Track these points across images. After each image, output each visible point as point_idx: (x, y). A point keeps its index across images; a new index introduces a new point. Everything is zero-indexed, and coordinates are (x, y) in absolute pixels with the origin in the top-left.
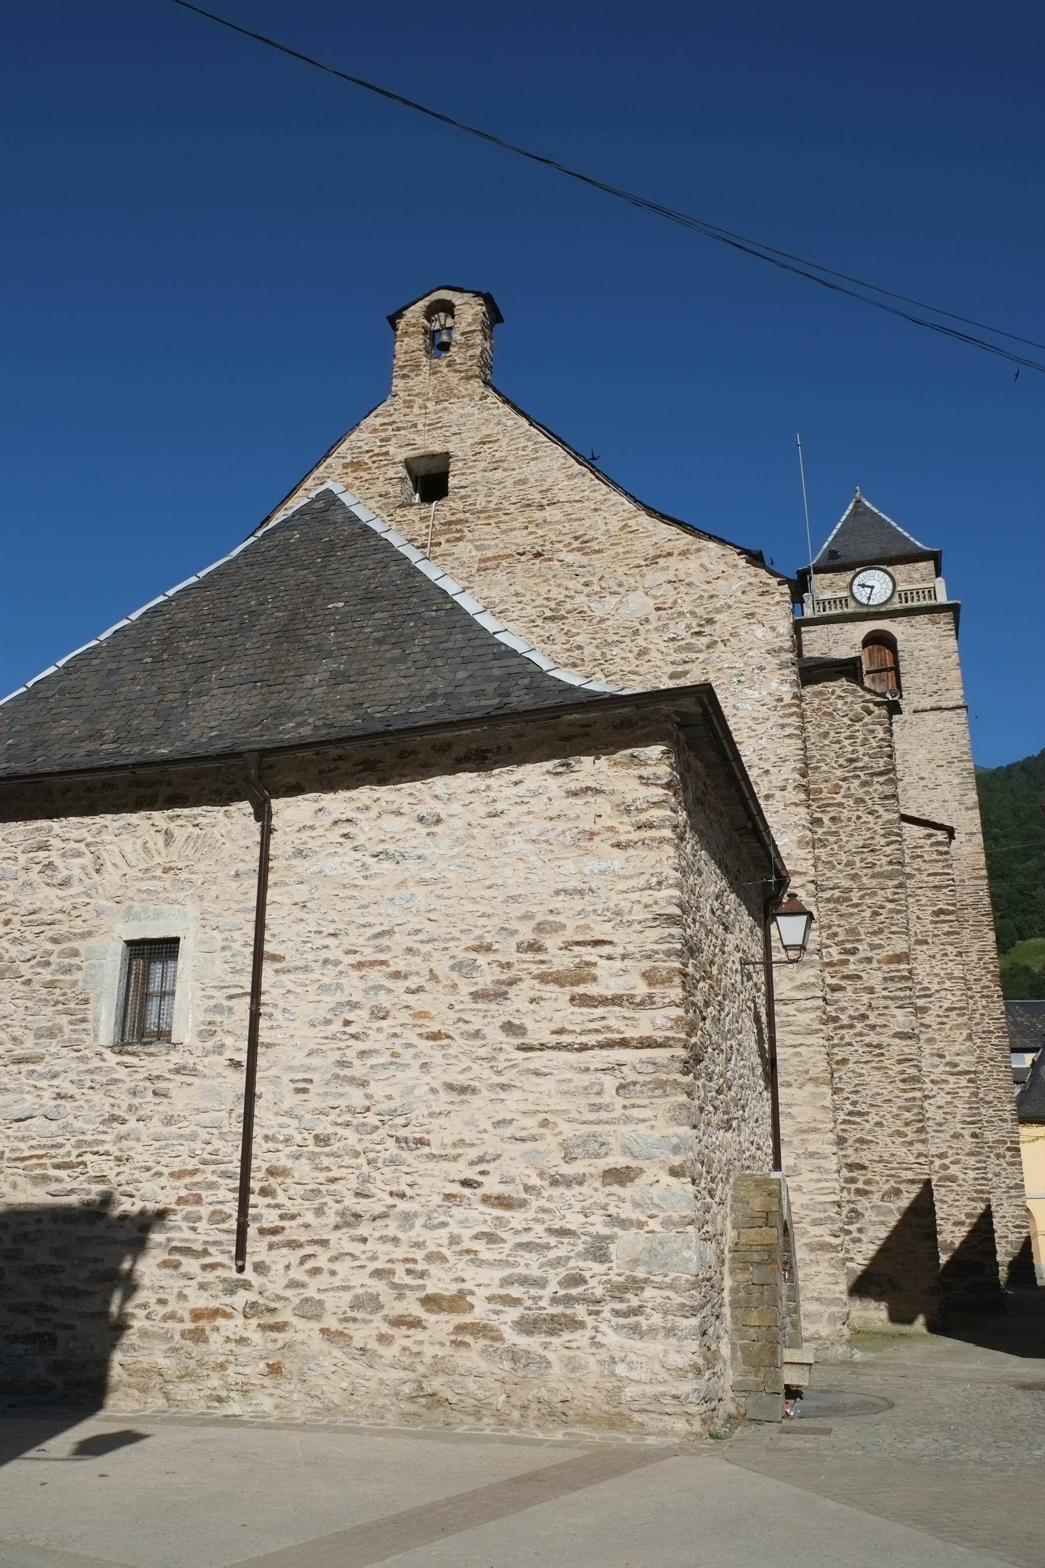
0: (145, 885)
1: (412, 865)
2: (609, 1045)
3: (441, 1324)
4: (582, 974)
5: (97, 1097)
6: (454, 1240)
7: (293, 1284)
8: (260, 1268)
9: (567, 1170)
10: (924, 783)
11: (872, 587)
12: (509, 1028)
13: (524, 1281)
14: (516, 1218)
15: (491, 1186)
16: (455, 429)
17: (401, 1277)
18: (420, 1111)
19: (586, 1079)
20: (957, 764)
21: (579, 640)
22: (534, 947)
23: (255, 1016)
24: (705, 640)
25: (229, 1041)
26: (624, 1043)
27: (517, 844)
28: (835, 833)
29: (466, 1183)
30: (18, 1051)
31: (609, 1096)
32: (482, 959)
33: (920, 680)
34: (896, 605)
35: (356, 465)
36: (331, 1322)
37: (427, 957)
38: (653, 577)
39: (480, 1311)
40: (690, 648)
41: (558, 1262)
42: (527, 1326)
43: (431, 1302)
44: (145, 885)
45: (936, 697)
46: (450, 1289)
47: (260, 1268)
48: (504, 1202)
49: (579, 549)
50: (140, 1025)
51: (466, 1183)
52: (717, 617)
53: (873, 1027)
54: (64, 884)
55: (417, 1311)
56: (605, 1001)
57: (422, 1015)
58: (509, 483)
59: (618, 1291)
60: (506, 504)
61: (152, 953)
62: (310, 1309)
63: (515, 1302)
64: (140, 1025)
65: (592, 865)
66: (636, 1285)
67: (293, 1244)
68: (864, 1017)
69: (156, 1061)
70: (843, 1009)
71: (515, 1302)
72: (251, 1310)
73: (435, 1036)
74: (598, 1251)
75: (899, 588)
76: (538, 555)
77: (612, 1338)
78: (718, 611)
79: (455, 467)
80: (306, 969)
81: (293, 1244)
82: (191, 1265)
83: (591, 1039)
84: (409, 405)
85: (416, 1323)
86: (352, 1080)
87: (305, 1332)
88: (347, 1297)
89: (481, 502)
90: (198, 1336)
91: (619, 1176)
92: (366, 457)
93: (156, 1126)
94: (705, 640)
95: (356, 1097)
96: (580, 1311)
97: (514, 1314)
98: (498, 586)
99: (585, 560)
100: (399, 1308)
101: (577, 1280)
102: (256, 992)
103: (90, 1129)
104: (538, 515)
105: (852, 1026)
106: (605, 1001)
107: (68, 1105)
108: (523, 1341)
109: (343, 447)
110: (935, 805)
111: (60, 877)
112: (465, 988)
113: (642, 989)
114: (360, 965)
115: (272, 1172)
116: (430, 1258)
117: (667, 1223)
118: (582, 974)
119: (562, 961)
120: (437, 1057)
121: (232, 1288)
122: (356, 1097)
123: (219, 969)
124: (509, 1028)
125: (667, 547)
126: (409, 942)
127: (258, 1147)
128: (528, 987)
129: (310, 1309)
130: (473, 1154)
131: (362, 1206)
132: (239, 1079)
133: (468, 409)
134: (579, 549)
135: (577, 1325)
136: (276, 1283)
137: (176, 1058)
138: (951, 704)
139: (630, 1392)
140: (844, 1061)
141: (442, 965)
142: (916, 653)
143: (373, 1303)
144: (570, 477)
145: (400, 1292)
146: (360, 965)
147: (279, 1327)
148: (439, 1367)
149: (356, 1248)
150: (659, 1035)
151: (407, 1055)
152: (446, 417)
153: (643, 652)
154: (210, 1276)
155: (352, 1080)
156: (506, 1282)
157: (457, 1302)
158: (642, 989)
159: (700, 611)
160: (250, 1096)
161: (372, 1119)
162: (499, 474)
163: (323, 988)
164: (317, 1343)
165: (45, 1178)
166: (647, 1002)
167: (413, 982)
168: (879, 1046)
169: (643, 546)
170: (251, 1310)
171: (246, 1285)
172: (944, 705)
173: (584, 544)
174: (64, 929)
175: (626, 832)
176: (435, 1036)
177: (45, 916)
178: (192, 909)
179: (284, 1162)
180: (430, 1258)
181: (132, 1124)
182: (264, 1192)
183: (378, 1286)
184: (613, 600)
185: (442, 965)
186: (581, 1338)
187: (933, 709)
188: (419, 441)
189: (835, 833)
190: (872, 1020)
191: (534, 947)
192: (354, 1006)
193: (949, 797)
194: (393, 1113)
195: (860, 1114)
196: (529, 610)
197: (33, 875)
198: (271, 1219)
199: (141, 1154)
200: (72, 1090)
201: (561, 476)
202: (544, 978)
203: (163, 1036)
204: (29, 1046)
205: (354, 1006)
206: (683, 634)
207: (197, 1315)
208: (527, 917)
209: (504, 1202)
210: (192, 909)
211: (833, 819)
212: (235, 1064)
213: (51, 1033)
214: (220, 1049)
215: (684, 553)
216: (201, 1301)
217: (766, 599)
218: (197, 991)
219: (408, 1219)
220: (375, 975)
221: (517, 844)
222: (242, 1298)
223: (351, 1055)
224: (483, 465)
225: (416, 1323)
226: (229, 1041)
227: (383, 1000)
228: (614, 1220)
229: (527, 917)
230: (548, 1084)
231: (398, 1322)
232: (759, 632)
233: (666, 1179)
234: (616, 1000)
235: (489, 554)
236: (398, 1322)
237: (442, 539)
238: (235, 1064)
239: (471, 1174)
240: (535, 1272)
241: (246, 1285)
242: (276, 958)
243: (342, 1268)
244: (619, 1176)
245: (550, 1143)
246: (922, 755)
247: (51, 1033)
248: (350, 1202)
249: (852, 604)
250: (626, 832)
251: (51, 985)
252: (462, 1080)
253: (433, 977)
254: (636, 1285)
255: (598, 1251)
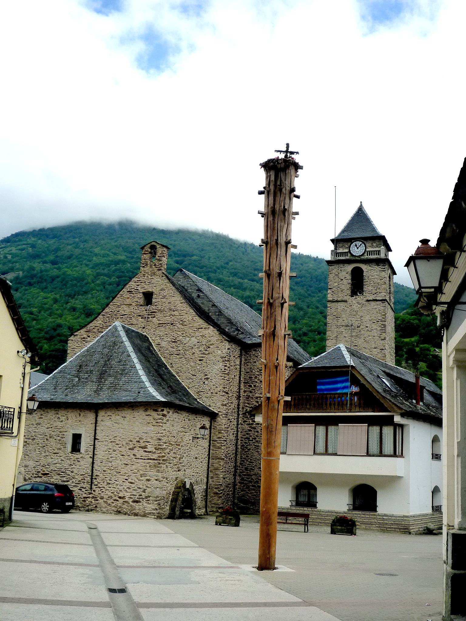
0: (76, 423)
1: (121, 425)
2: (148, 459)
3: (121, 501)
4: (145, 447)
5: (68, 461)
6: (124, 488)
7: (99, 494)
8: (94, 491)
9: (141, 478)
10: (367, 329)
11: (358, 248)
12: (134, 455)
13: (133, 495)
14: (133, 485)
15: (130, 480)
16: (155, 285)
17: (115, 493)
18: (119, 468)
19: (145, 464)
20: (380, 322)
21: (180, 348)
22: (138, 442)
23: (94, 449)
24: (207, 352)
25: (90, 453)
26: (151, 459)
27: (137, 423)
28: (254, 390)
29: (126, 479)
30: (54, 452)
31: (148, 468)
32: (131, 443)
33: (370, 288)
34: (366, 257)
35: (130, 292)
36: (105, 500)
37: (122, 442)
38: (197, 334)
39: (127, 499)
40: (204, 354)
41: (138, 493)
42: (134, 501)
43: (120, 497)
44: (76, 423)
45: (375, 295)
46: (122, 496)
47: (94, 491)
48: (131, 483)
49: (182, 324)
50: (76, 448)
51: (126, 479)
52: (211, 346)
53: (257, 441)
54: (62, 421)
55: (118, 499)
56: (149, 452)
57: (121, 451)
58: (167, 303)
59: (146, 497)
60: (165, 309)
61: (77, 438)
62: (102, 498)
63: (132, 498)
64: (76, 448)
65: (149, 428)
66: (149, 497)
67: (99, 487)
68: (255, 439)
69: (77, 455)
70: (251, 436)
71: (132, 498)
72: (93, 498)
73: (123, 455)
74: (144, 491)
75: (367, 250)
76: (172, 324)
77: (145, 504)
78: (211, 345)
79: (154, 296)
80: (102, 442)
81: (99, 487)
82: (83, 490)
83: (146, 458)
84: (144, 275)
85: (117, 500)
86: (109, 461)
87: (101, 501)
88: (107, 496)
89: (160, 307)
90: (84, 501)
91: (148, 480)
92: (133, 290)
93: (78, 467)
94: (207, 352)
95: (110, 464)
96: (141, 500)
97: (132, 500)
98: (161, 331)
99: (183, 327)
100: (115, 498)
101: (141, 495)
102: (94, 445)
103: (67, 466)
104: (173, 313)
105: (252, 441)
106: (149, 452)
107: (63, 462)
108: (132, 504)
109: (127, 286)
110: (370, 337)
111: (61, 420)
112: (128, 448)
113: (154, 450)
114: (111, 442)
115: (96, 476)
116: (120, 491)
117: (154, 488)
118: (145, 447)
119: (143, 445)
120: (123, 459)
121: (90, 493)
122: (110, 464)
123: (88, 440)
124: (134, 455)
125: (202, 326)
126: (119, 439)
127: (94, 471)
128: (137, 448)
129: (102, 498)
130: (127, 475)
131: (110, 482)
132: (91, 460)
133: (159, 280)
134: (182, 324)
135: (140, 502)
136: (96, 493)
137: (81, 455)
138: (380, 298)
139: (147, 512)
140: (250, 449)
141: (124, 443)
142: (370, 277)
143: (111, 497)
144: (181, 303)
145: (115, 496)
146: (111, 442)
147: (97, 500)
148: (120, 507)
149: (109, 489)
150: (156, 458)
151: (118, 458)
152: (153, 281)
153: (194, 353)
154: (86, 492)
155: (109, 461)
156: (131, 495)
157: (123, 498)
158: (154, 450)
159: (207, 344)
160: (93, 463)
161: (112, 468)
162: (164, 300)
163: (106, 446)
164: (103, 503)
165: (59, 474)
166: (155, 453)
167: (120, 446)
168: (258, 446)
169: (196, 325)
170: (93, 498)
171: (92, 493)
172: (378, 298)
173: (183, 323)
174: (62, 430)
175: (154, 424)
176: (123, 455)
177: (58, 427)
178: (84, 429)
179: (98, 474)
180: (120, 491)
181: (74, 466)
182: (95, 479)
183: (112, 495)
184: (188, 339)
185: (124, 443)
186: (141, 504)
187: (374, 300)
188: (146, 287)
189: (254, 390)
190: (257, 439)
191: (138, 442)
192: (110, 449)
193: (376, 334)
194: (116, 467)
195: (252, 462)
196: (169, 339)
197: (56, 419)
198: (96, 483)
199: (75, 471)
200: (64, 459)
201: (179, 302)
202: (140, 447)
203: (79, 451)
204: (56, 451)
205: (110, 449)
206: (203, 350)
207: (84, 498)
208: (138, 436)
209: (131, 483)
210: (84, 429)
211: (255, 386)
212: (91, 457)
213: (60, 449)
214: (88, 454)
215: (205, 328)
216: (85, 496)
217: (221, 344)
218: (85, 444)
219: (117, 485)
220: (113, 444)
221: (137, 423)
222: (91, 496)
223: (109, 457)
224: (161, 296)
225: (117, 500)
226: (90, 453)
227: (115, 448)
228: (147, 487)
229: (138, 436)
230: (139, 465)
231: (115, 500)
232: (219, 352)
233: (155, 481)
234: (150, 452)
235: (161, 322)
236: (115, 500)
237: (150, 316)
238: (91, 457)
239: (127, 478)
240: (135, 494)
241: (92, 493)
242: (98, 439)
243: (107, 492)
244: (148, 480)
245: (139, 474)
246: (368, 317)
247: (60, 449)
248: (108, 481)
249: (349, 255)
250: (154, 424)
251: (60, 440)
252: (126, 463)
253: (123, 445)
254: (149, 497)
255: (144, 491)
